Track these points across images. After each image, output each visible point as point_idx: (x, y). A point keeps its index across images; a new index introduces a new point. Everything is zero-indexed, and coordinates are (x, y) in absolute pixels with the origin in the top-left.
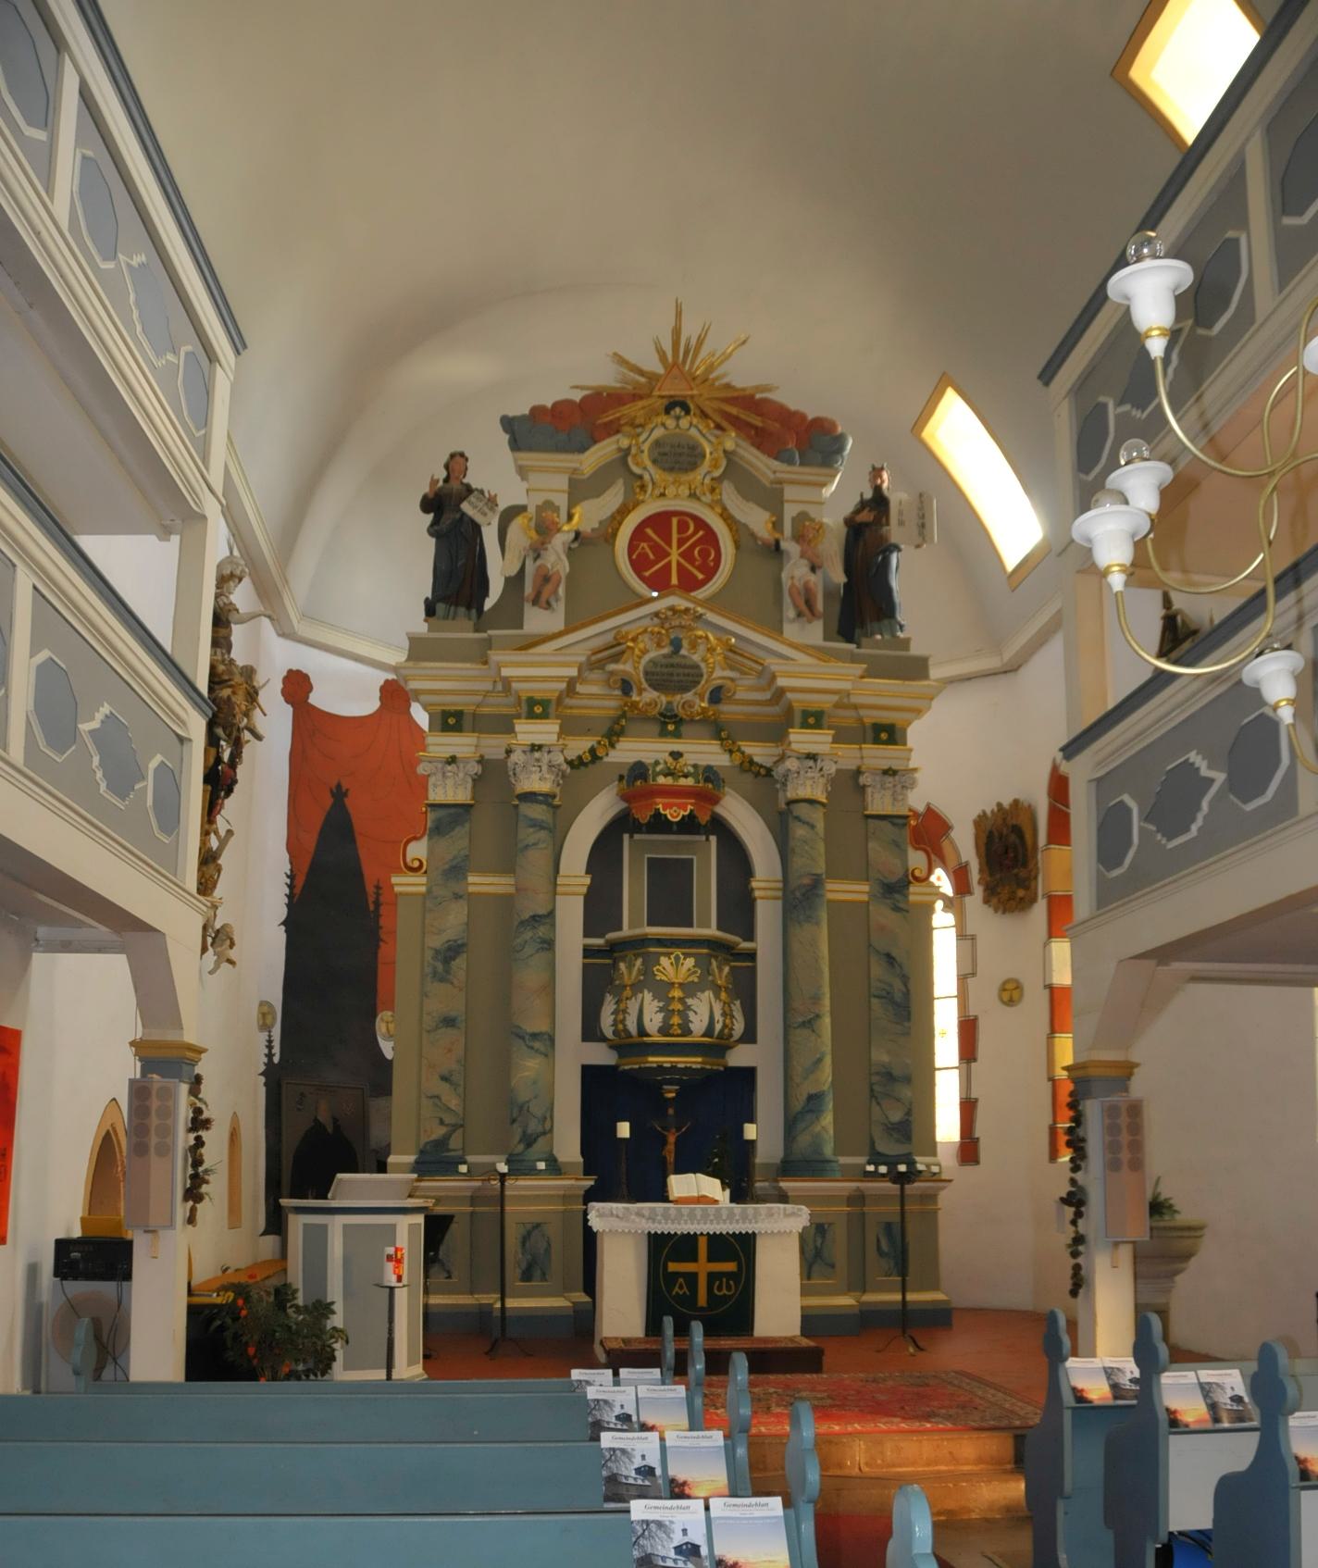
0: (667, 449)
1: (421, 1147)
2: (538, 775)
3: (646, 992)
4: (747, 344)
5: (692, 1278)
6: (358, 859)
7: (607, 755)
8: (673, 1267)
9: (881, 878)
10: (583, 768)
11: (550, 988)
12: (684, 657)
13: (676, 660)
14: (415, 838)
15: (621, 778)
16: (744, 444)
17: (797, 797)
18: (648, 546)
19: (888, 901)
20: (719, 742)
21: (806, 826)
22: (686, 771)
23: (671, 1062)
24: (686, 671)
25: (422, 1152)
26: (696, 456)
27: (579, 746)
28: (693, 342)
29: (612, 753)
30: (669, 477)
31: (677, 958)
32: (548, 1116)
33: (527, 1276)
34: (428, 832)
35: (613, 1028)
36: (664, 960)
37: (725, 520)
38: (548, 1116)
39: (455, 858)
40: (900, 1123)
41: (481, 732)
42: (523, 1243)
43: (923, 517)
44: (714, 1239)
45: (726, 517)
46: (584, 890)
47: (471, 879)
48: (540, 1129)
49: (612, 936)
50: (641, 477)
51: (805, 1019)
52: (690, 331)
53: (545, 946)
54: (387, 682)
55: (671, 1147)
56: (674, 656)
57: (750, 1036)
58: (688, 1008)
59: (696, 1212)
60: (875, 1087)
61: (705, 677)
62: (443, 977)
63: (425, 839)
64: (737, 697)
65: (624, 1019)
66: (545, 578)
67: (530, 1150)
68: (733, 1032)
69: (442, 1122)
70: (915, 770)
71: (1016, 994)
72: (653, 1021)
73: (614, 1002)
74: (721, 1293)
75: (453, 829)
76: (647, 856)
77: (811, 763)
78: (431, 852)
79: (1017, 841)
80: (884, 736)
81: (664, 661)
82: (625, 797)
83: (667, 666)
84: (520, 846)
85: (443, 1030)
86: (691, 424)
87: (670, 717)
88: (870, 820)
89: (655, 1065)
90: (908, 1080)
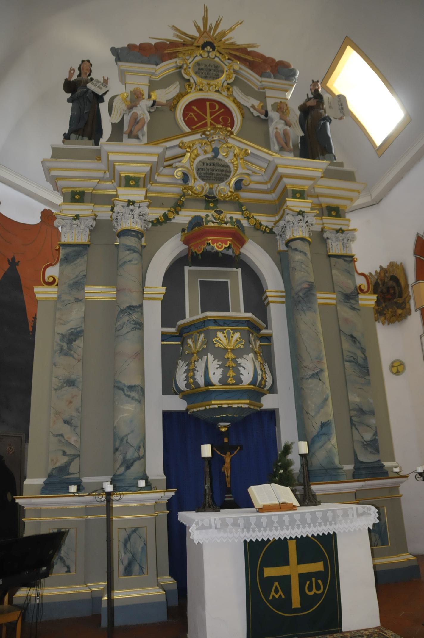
0: (203, 67)
1: (49, 472)
2: (132, 220)
3: (209, 354)
4: (242, 24)
5: (285, 581)
6: (23, 301)
7: (174, 218)
8: (269, 572)
9: (343, 291)
10: (159, 226)
11: (140, 355)
12: (220, 160)
13: (215, 161)
14: (51, 265)
15: (183, 230)
16: (244, 67)
17: (293, 238)
18: (194, 114)
19: (348, 304)
20: (241, 213)
21: (301, 253)
22: (226, 220)
23: (228, 404)
24: (222, 168)
25: (50, 476)
26: (219, 71)
27: (157, 213)
28: (214, 25)
29: (177, 217)
30: (205, 82)
31: (228, 333)
32: (141, 445)
33: (128, 571)
34: (60, 261)
35: (186, 382)
36: (220, 334)
37: (235, 104)
38: (142, 445)
39: (77, 276)
40: (371, 441)
41: (95, 204)
42: (125, 545)
43: (342, 105)
44: (301, 542)
45: (235, 101)
46: (161, 297)
47: (88, 289)
48: (136, 455)
49: (180, 323)
50: (188, 80)
51: (314, 373)
52: (212, 21)
53: (138, 326)
54: (45, 210)
55: (227, 465)
56: (215, 159)
57: (273, 390)
58: (239, 365)
59: (284, 519)
60: (353, 418)
61: (232, 173)
62: (66, 352)
63: (58, 265)
64: (249, 187)
65: (194, 374)
66: (135, 121)
67: (129, 471)
68: (267, 383)
69: (64, 453)
70: (354, 230)
71: (400, 368)
72: (215, 375)
73: (185, 364)
74: (312, 593)
75: (76, 259)
76: (199, 279)
77: (300, 217)
78: (61, 273)
79: (394, 284)
80: (333, 213)
81: (209, 162)
82: (186, 241)
83: (210, 165)
84: (120, 263)
85: (67, 387)
86: (216, 56)
87: (212, 198)
88: (332, 258)
89: (216, 406)
90: (372, 413)
